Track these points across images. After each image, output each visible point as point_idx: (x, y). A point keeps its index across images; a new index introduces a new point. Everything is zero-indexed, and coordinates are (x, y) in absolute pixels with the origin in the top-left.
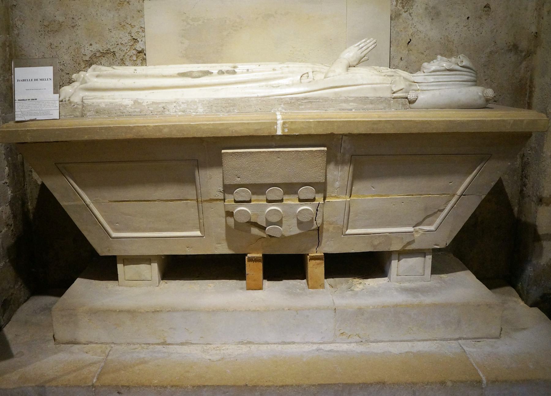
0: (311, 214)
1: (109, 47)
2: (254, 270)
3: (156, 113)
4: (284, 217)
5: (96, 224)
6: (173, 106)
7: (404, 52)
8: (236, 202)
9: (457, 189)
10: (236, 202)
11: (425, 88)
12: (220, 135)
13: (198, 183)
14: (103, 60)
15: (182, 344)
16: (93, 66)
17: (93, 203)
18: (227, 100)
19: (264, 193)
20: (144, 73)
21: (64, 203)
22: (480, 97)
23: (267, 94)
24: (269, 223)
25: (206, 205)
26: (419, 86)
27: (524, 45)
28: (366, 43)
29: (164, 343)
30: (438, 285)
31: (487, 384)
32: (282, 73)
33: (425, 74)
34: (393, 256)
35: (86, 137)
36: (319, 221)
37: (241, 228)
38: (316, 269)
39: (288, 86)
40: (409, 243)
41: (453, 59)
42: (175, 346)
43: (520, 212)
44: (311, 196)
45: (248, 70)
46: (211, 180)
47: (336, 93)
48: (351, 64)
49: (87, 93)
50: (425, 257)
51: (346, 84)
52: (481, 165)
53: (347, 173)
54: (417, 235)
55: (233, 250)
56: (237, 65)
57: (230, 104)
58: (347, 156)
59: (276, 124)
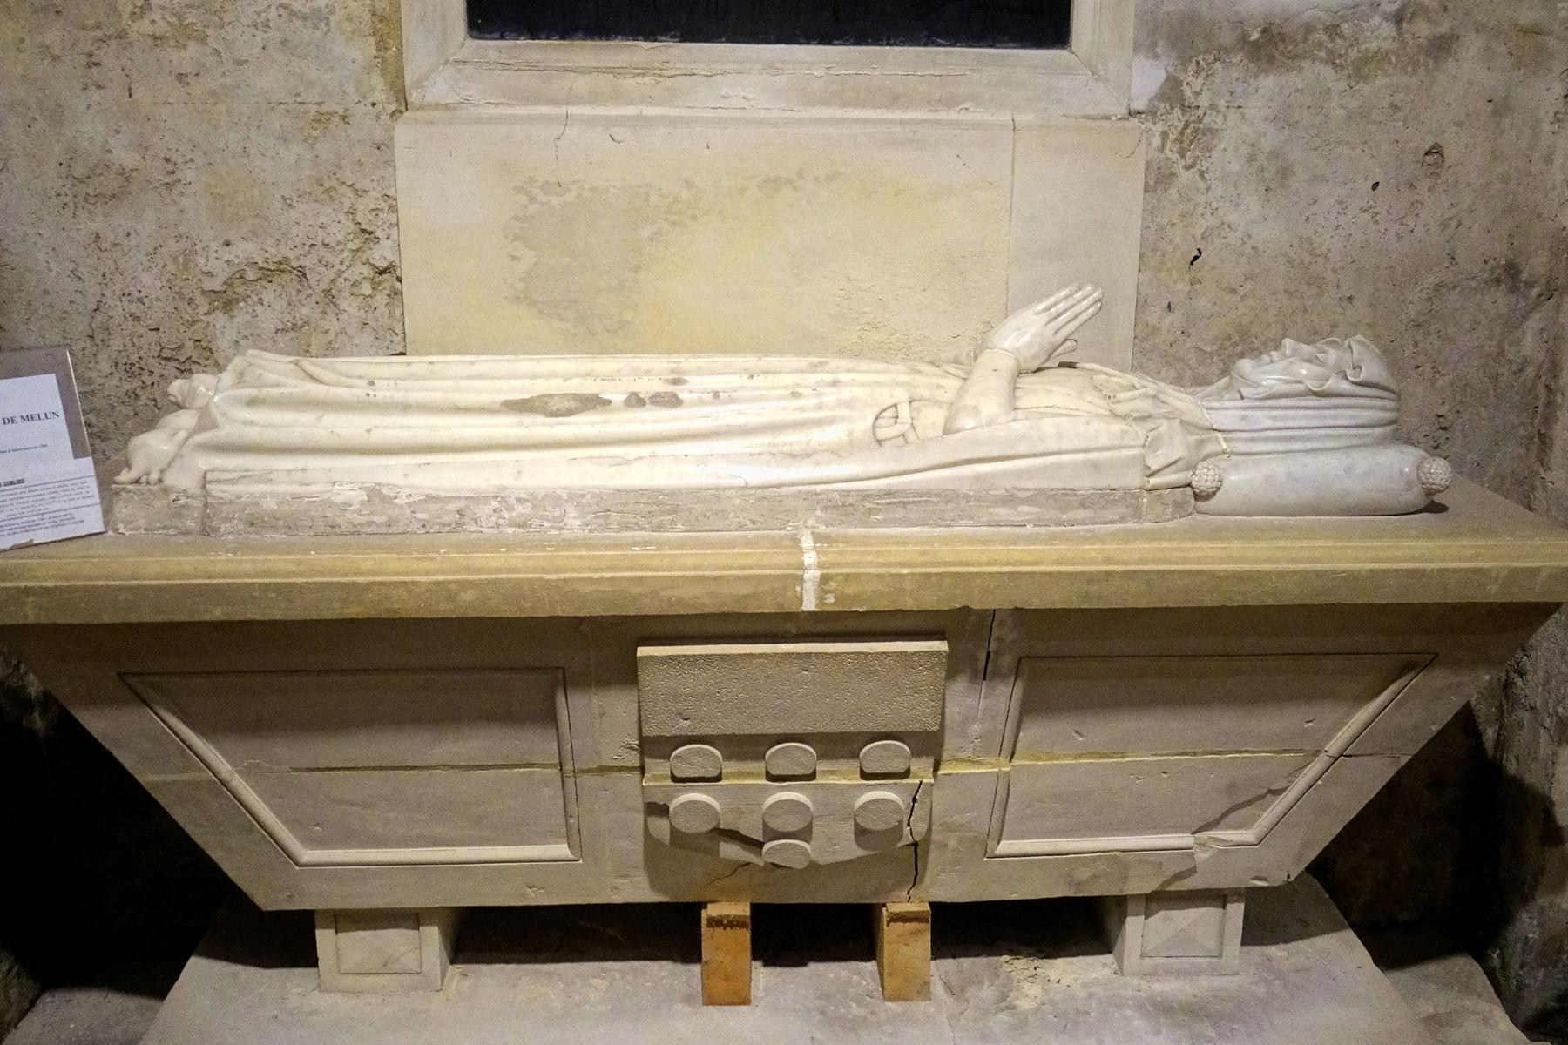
0: (898, 810)
1: (285, 251)
3: (436, 528)
4: (818, 818)
5: (251, 829)
6: (488, 509)
7: (1180, 286)
8: (675, 779)
9: (1329, 736)
10: (675, 779)
11: (1241, 447)
13: (564, 729)
17: (240, 773)
18: (652, 494)
19: (760, 757)
21: (147, 778)
22: (1410, 485)
25: (587, 781)
26: (1226, 440)
27: (1537, 264)
28: (1071, 301)
30: (1261, 990)
32: (820, 407)
33: (1245, 403)
34: (1131, 907)
35: (218, 614)
39: (837, 452)
40: (1179, 876)
43: (1500, 743)
44: (897, 766)
45: (716, 395)
46: (603, 720)
47: (978, 478)
48: (1024, 366)
49: (219, 461)
50: (1224, 907)
51: (1010, 452)
53: (1002, 703)
54: (1201, 856)
55: (665, 893)
57: (663, 506)
58: (1007, 660)
59: (800, 580)
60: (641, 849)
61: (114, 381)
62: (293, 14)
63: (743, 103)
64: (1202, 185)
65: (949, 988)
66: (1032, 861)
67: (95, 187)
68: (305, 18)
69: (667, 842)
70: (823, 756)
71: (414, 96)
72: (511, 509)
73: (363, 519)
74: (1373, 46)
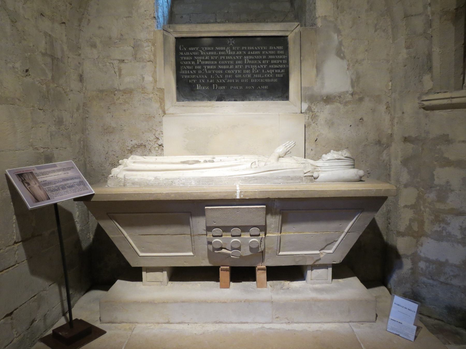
0: (257, 243)
1: (142, 142)
2: (225, 275)
6: (177, 181)
8: (213, 236)
9: (345, 229)
10: (213, 236)
12: (204, 199)
14: (139, 150)
19: (230, 231)
21: (111, 236)
22: (356, 175)
25: (196, 237)
27: (384, 140)
29: (168, 323)
32: (240, 162)
35: (126, 199)
36: (262, 247)
38: (261, 275)
40: (317, 260)
41: (340, 152)
42: (175, 325)
44: (257, 233)
46: (199, 224)
47: (271, 174)
56: (215, 156)
57: (210, 180)
59: (236, 192)
60: (207, 253)
64: (316, 126)
65: (271, 286)
66: (287, 256)
67: (108, 131)
71: (167, 112)
72: (181, 181)
74: (348, 100)
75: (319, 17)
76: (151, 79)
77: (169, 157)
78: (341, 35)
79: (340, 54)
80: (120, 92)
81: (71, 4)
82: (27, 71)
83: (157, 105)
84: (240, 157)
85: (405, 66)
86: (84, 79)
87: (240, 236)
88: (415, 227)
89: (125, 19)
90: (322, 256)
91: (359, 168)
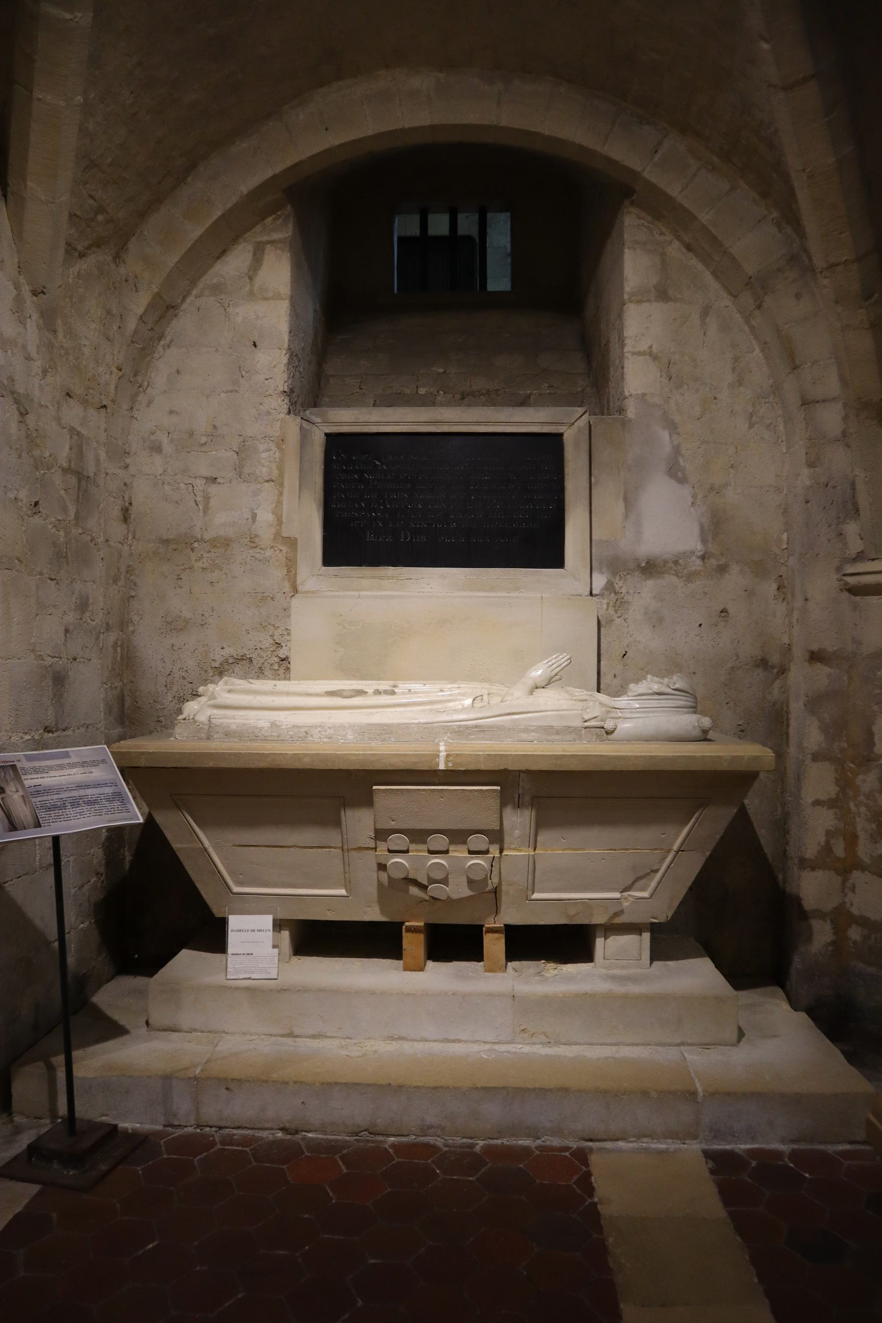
4: (452, 872)
6: (317, 731)
8: (390, 851)
9: (673, 843)
10: (390, 851)
12: (371, 768)
15: (313, 1037)
16: (225, 678)
18: (381, 726)
19: (424, 842)
20: (285, 689)
21: (176, 845)
22: (694, 727)
23: (430, 721)
24: (432, 881)
25: (354, 854)
27: (775, 658)
29: (291, 1035)
31: (704, 1096)
34: (598, 933)
35: (211, 764)
36: (495, 880)
37: (398, 886)
38: (494, 945)
40: (616, 915)
41: (666, 680)
44: (483, 847)
45: (410, 690)
46: (359, 823)
47: (513, 721)
48: (538, 684)
49: (216, 711)
50: (641, 935)
51: (525, 710)
52: (700, 811)
53: (528, 818)
54: (626, 904)
57: (385, 730)
58: (527, 798)
59: (438, 756)
61: (173, 704)
62: (256, 559)
63: (431, 590)
64: (625, 624)
66: (549, 902)
67: (175, 625)
68: (260, 560)
69: (386, 885)
70: (451, 842)
71: (300, 588)
72: (326, 731)
73: (269, 734)
74: (693, 569)
75: (631, 395)
76: (270, 517)
77: (302, 682)
78: (678, 434)
79: (676, 473)
80: (205, 545)
81: (121, 370)
82: (36, 504)
83: (279, 573)
84: (450, 686)
85: (807, 502)
86: (133, 516)
87: (447, 852)
88: (839, 850)
89: (223, 395)
90: (626, 904)
91: (703, 713)
